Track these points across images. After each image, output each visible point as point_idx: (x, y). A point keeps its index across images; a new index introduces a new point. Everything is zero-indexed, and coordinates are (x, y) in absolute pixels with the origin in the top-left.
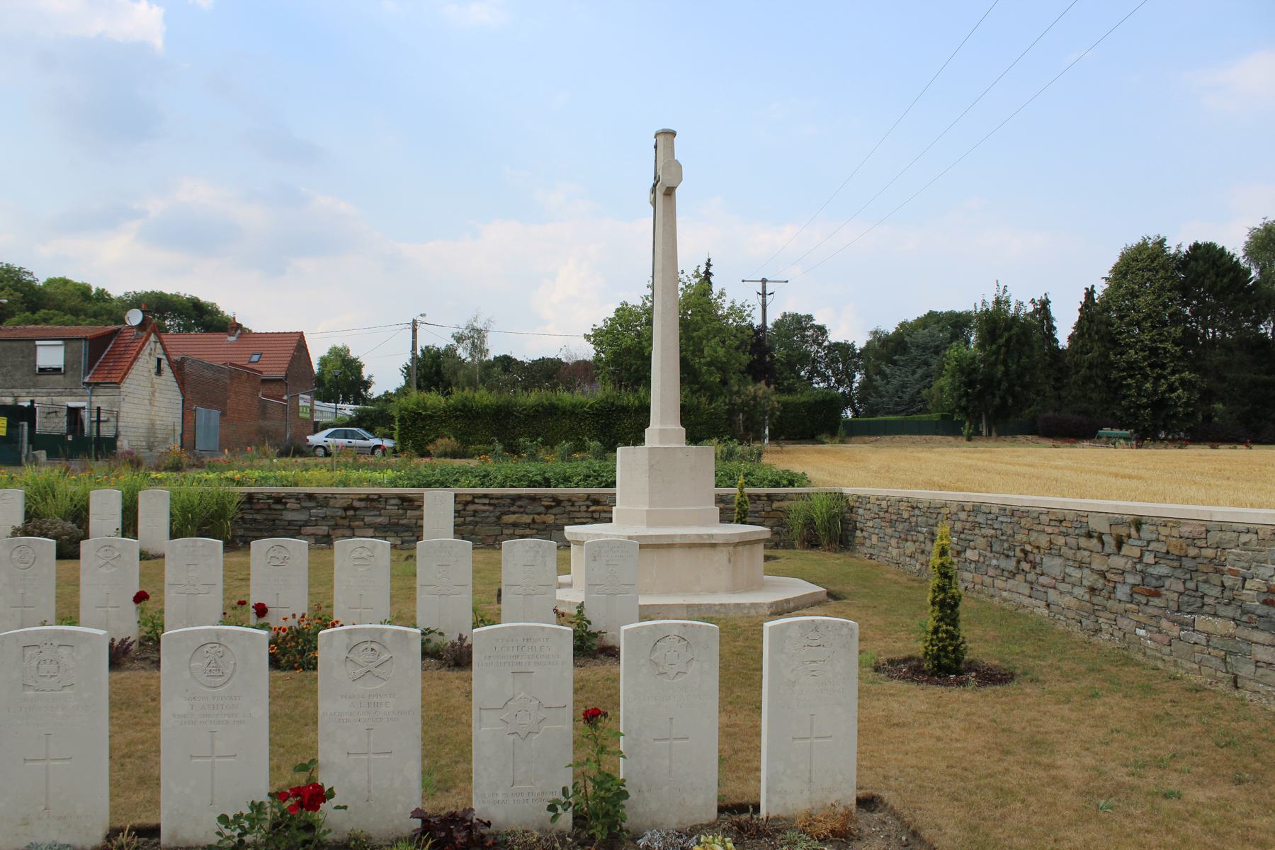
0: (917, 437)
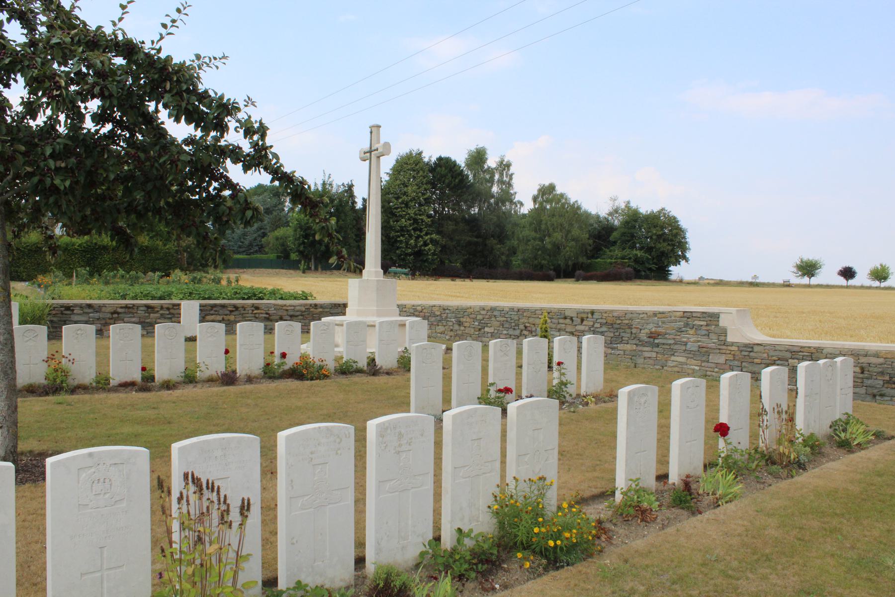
0: (270, 270)
